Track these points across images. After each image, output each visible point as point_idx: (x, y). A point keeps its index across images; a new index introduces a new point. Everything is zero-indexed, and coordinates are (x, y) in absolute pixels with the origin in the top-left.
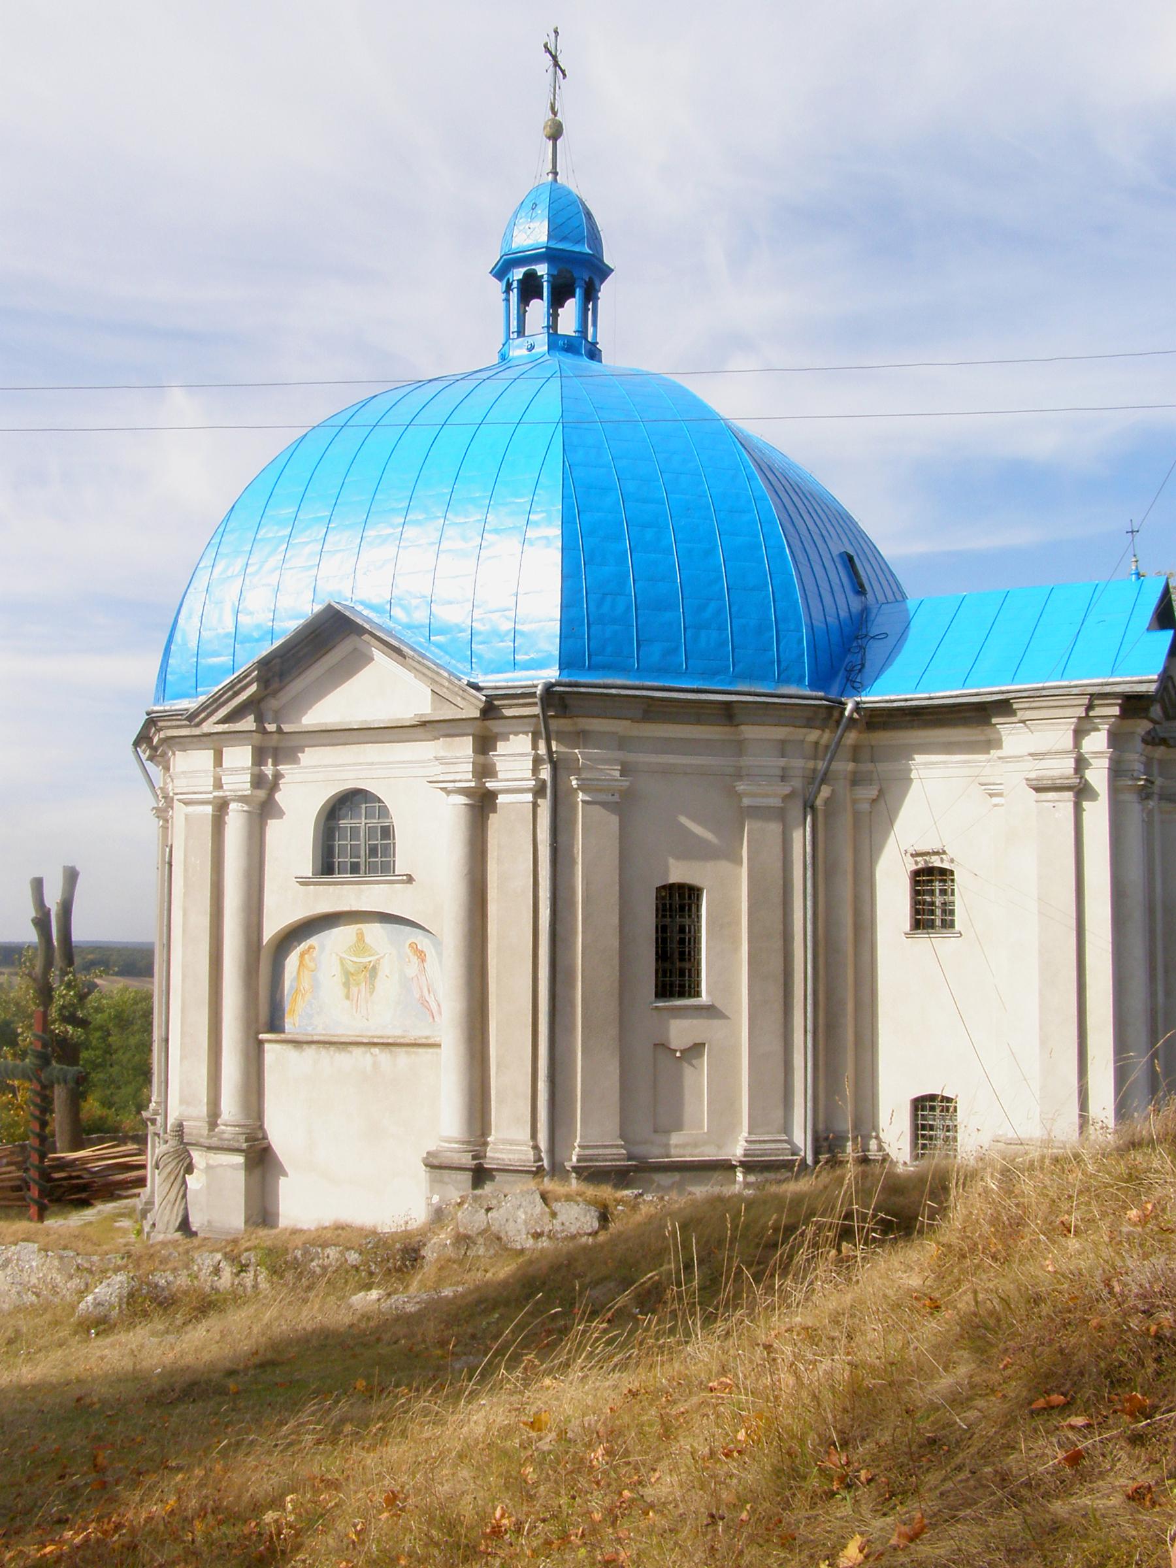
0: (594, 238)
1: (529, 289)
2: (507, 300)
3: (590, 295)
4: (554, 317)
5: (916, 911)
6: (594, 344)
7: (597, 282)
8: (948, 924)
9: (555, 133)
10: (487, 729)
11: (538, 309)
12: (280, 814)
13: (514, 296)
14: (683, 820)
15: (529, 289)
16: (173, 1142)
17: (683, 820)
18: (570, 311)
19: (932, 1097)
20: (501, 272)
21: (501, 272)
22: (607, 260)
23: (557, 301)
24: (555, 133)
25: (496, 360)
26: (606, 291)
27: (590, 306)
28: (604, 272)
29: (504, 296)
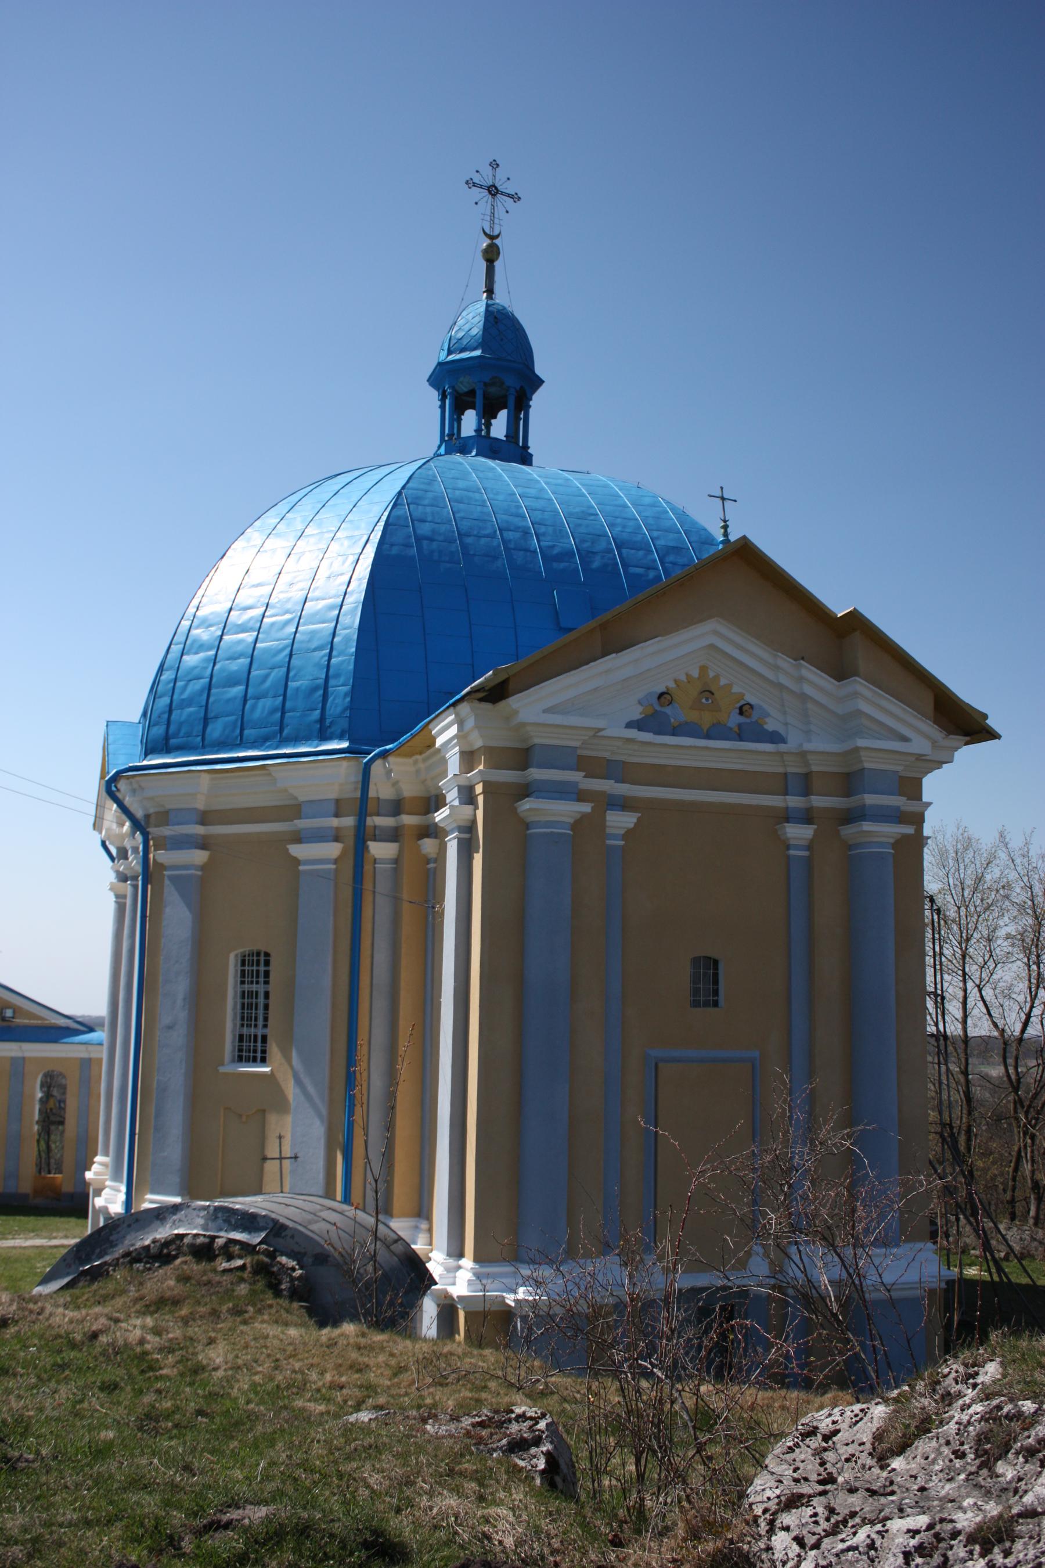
3: (520, 405)
6: (526, 447)
9: (491, 255)
24: (491, 255)
26: (537, 401)
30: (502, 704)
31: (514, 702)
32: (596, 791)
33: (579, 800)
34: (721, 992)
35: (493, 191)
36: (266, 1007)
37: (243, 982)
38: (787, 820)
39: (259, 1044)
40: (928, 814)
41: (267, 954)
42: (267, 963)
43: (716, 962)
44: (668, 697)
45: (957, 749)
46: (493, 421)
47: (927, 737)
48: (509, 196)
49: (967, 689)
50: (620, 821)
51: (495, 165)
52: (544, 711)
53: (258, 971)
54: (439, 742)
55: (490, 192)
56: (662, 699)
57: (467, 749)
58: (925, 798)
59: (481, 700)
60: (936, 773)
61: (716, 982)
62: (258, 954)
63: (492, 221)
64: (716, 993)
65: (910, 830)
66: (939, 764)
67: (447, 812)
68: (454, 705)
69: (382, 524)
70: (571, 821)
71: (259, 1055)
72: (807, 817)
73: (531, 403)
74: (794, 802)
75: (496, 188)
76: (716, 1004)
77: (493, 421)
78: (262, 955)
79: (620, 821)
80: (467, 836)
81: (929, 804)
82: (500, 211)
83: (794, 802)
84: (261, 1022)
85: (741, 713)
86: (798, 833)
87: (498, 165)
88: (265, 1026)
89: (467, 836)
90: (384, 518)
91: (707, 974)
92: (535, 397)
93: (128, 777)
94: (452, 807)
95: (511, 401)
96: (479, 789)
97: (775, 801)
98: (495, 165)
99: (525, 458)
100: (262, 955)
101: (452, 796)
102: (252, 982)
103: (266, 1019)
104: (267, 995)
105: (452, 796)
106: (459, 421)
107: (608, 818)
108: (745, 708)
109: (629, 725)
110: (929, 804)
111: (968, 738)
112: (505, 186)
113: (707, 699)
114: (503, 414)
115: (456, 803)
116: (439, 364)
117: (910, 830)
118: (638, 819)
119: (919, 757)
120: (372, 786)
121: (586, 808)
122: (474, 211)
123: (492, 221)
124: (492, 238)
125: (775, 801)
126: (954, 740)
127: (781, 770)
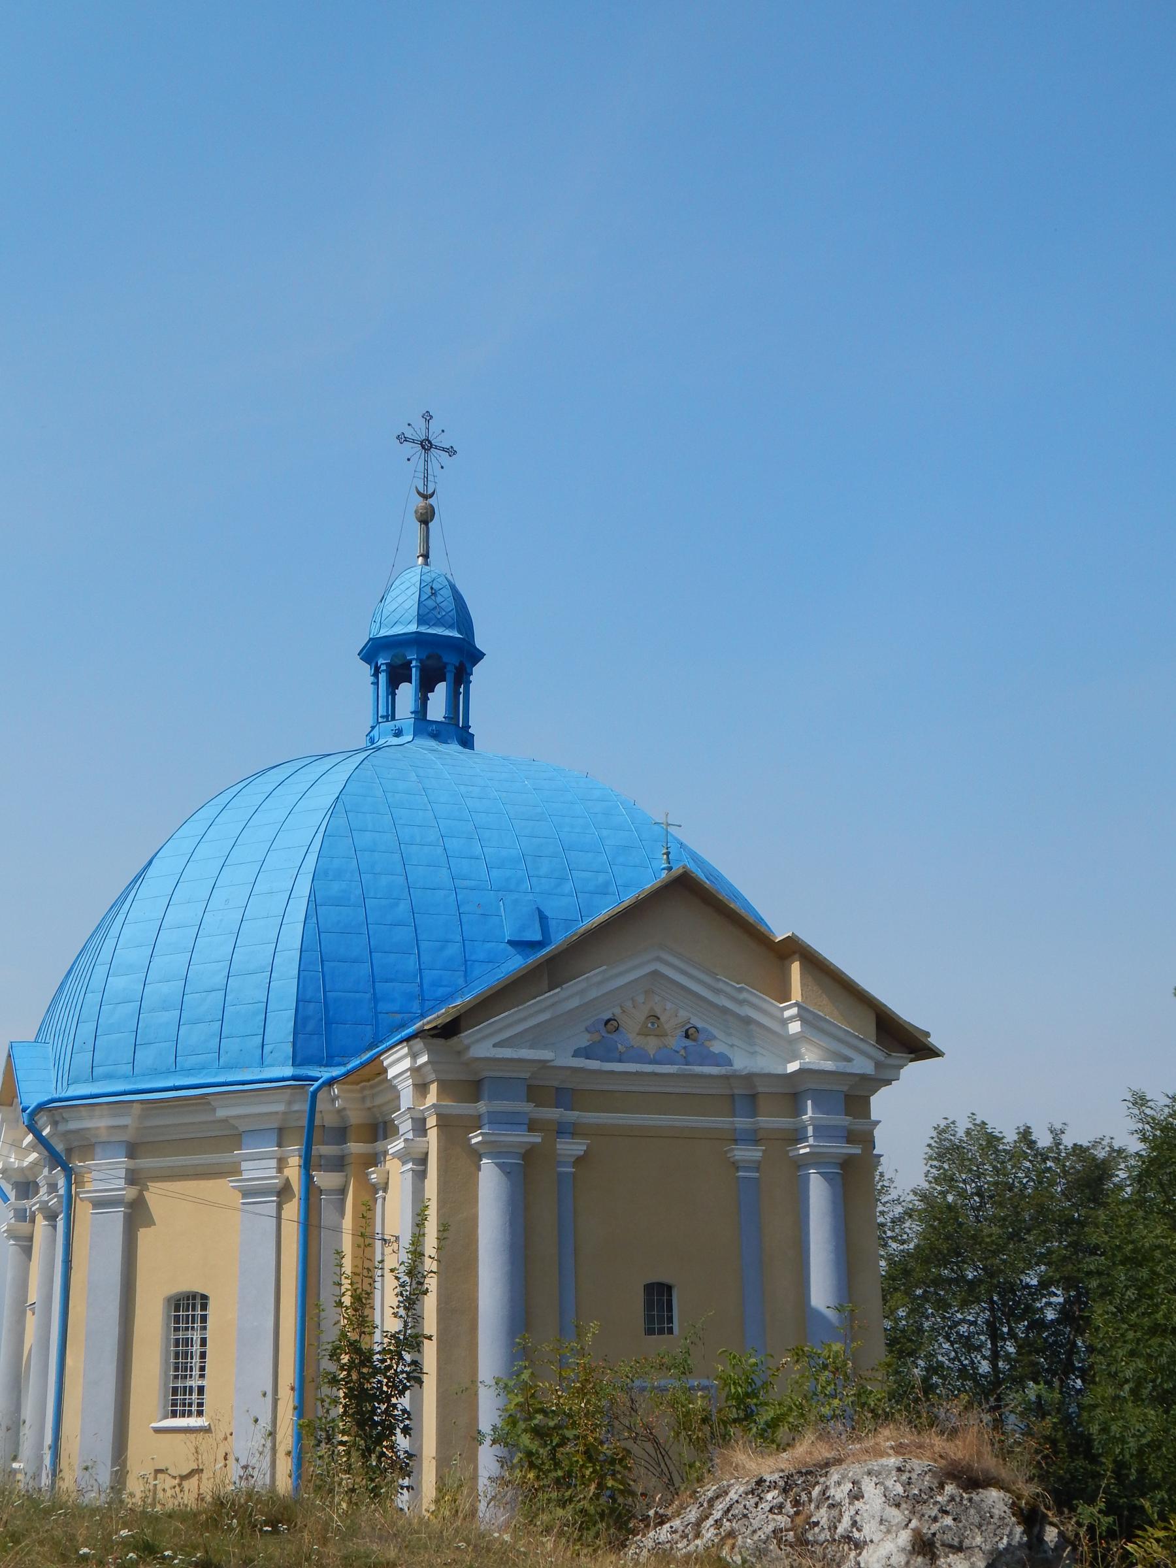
0: (463, 620)
1: (398, 675)
2: (376, 684)
3: (461, 679)
4: (423, 702)
5: (649, 1319)
6: (467, 727)
7: (468, 665)
8: (650, 1331)
9: (426, 518)
10: (342, 1150)
11: (407, 693)
12: (149, 1222)
13: (382, 677)
14: (809, 1102)
15: (398, 675)
16: (405, 1257)
17: (809, 1102)
18: (439, 697)
19: (194, 1296)
20: (370, 653)
21: (370, 653)
22: (479, 644)
23: (426, 687)
24: (426, 518)
25: (363, 742)
26: (479, 673)
27: (461, 690)
28: (476, 656)
29: (372, 679)
30: (455, 1039)
31: (466, 1036)
32: (477, 1276)
33: (530, 1130)
34: (675, 1319)
35: (427, 445)
36: (203, 1355)
37: (177, 1329)
38: (735, 1141)
39: (195, 1396)
40: (877, 1132)
41: (204, 1297)
42: (204, 1307)
43: (669, 1288)
44: (615, 1023)
45: (902, 1067)
46: (430, 695)
47: (869, 1057)
48: (443, 450)
49: (908, 1009)
50: (571, 1148)
51: (428, 417)
52: (494, 1046)
53: (193, 1316)
54: (391, 1073)
55: (423, 447)
56: (609, 1026)
57: (420, 1081)
58: (874, 1116)
59: (433, 1036)
60: (884, 1090)
61: (670, 1309)
62: (194, 1297)
63: (426, 478)
64: (670, 1320)
65: (856, 1150)
66: (888, 1082)
67: (402, 1145)
68: (408, 1039)
69: (320, 835)
70: (523, 1151)
71: (194, 1408)
72: (754, 1138)
73: (471, 678)
74: (742, 1122)
75: (430, 442)
76: (670, 1331)
77: (430, 695)
78: (198, 1298)
79: (571, 1148)
80: (421, 1168)
81: (878, 1122)
82: (434, 466)
83: (742, 1122)
84: (196, 1372)
85: (687, 1036)
86: (745, 1153)
87: (431, 417)
88: (202, 1376)
89: (421, 1168)
90: (323, 828)
91: (659, 1298)
92: (476, 669)
93: (50, 1110)
94: (406, 1140)
95: (450, 676)
96: (432, 1121)
97: (722, 1122)
98: (428, 417)
99: (467, 741)
100: (198, 1298)
101: (405, 1126)
102: (187, 1329)
103: (202, 1369)
104: (204, 1342)
105: (405, 1126)
106: (394, 695)
107: (558, 1146)
108: (691, 1031)
109: (577, 1054)
110: (878, 1122)
111: (912, 1056)
112: (438, 439)
113: (653, 1024)
114: (441, 688)
115: (410, 1136)
116: (370, 639)
117: (856, 1150)
118: (588, 1146)
119: (863, 1078)
120: (317, 1116)
121: (536, 1138)
122: (406, 467)
123: (426, 478)
124: (425, 497)
125: (722, 1122)
126: (897, 1057)
127: (728, 1092)
